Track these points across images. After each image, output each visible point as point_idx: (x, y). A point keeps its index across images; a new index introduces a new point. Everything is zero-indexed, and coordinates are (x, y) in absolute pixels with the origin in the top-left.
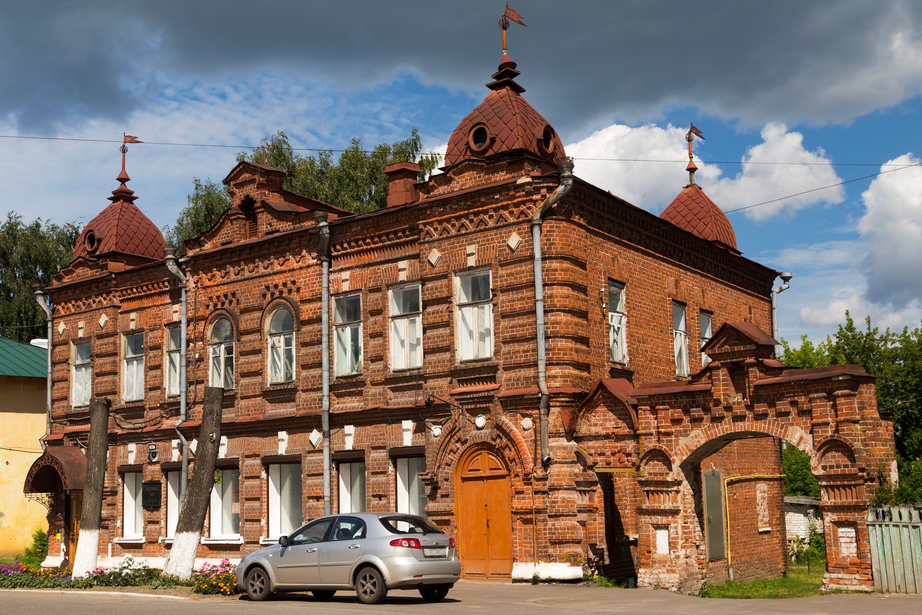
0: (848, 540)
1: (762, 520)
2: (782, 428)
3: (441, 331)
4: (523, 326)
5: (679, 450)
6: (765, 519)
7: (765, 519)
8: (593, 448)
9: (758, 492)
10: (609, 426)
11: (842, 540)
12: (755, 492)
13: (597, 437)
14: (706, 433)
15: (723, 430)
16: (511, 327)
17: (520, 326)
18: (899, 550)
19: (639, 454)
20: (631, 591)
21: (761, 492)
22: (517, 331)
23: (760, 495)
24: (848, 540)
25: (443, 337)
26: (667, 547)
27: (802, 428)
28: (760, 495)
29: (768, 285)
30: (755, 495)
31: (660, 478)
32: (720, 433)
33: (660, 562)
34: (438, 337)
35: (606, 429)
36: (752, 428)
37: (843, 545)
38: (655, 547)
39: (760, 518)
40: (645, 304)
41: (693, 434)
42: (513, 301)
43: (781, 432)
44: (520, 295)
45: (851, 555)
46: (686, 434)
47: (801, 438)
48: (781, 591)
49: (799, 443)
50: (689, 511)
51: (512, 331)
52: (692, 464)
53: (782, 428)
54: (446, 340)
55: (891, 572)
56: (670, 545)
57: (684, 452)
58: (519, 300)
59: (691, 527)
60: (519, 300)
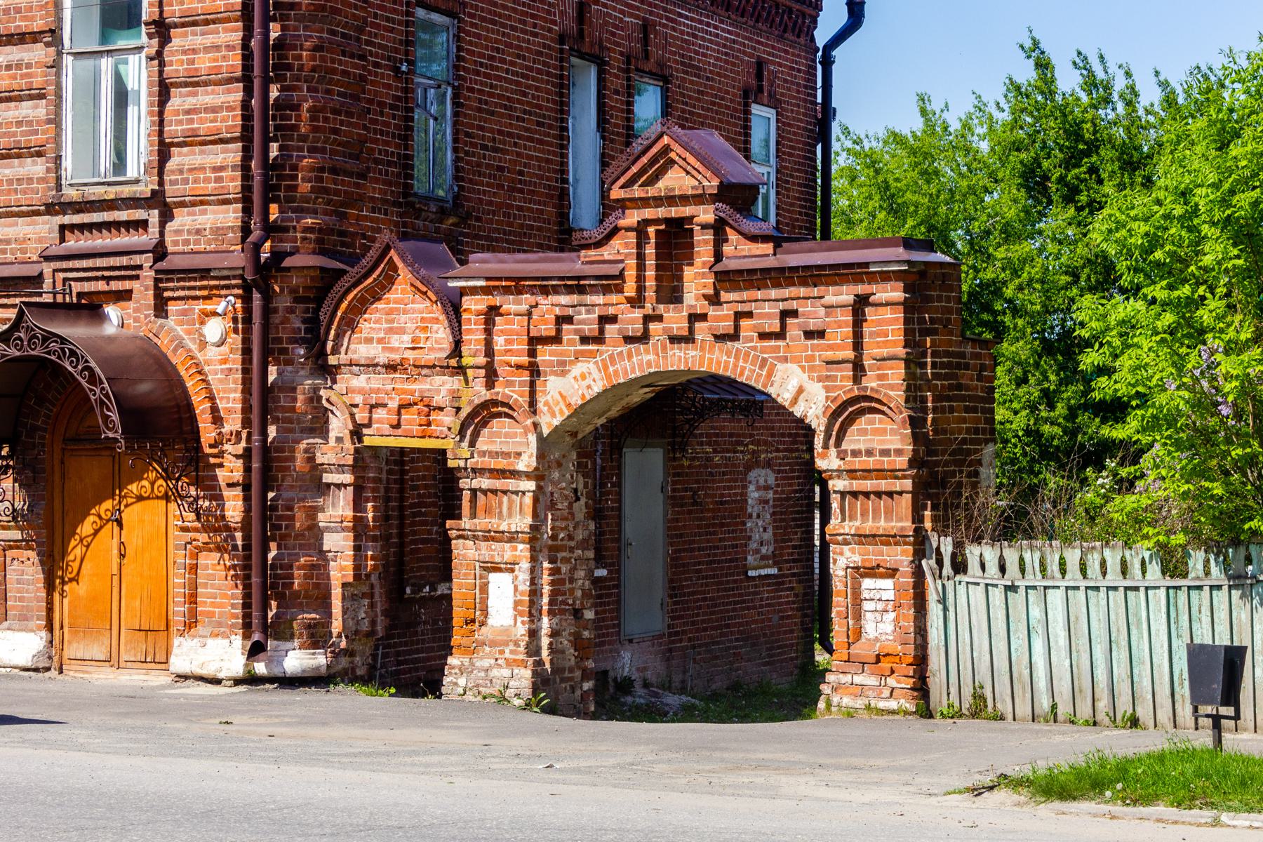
0: (880, 606)
1: (757, 551)
2: (761, 367)
3: (26, 110)
4: (214, 110)
5: (546, 404)
6: (764, 550)
7: (764, 550)
8: (361, 391)
9: (752, 488)
10: (397, 345)
11: (867, 606)
12: (745, 487)
13: (371, 366)
14: (606, 368)
15: (641, 365)
16: (188, 112)
17: (206, 110)
18: (1104, 625)
19: (458, 409)
20: (429, 701)
21: (758, 488)
22: (201, 121)
23: (756, 495)
24: (880, 606)
25: (30, 123)
26: (511, 612)
27: (803, 368)
28: (756, 495)
29: (810, 11)
30: (744, 496)
31: (501, 463)
32: (633, 371)
33: (493, 644)
34: (19, 124)
35: (392, 350)
36: (701, 365)
37: (868, 615)
38: (485, 612)
39: (753, 546)
40: (503, 61)
41: (578, 369)
42: (194, 51)
43: (759, 375)
44: (209, 40)
45: (883, 638)
46: (562, 368)
47: (800, 391)
48: (673, 700)
49: (795, 401)
50: (562, 535)
51: (191, 121)
52: (574, 434)
53: (761, 367)
54: (36, 132)
55: (1121, 670)
56: (515, 609)
57: (557, 410)
58: (207, 49)
59: (564, 570)
60: (207, 49)
